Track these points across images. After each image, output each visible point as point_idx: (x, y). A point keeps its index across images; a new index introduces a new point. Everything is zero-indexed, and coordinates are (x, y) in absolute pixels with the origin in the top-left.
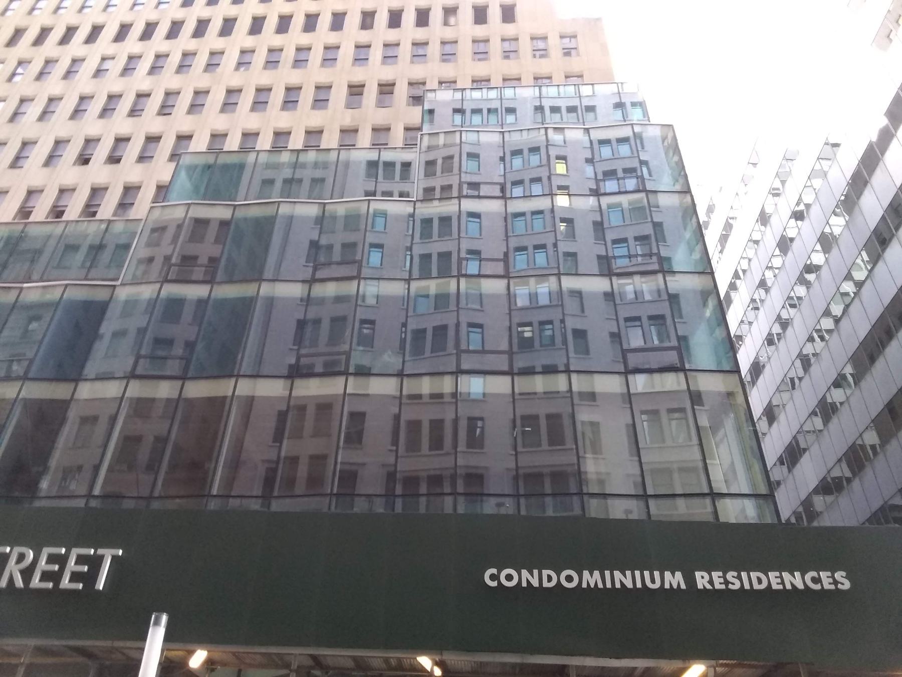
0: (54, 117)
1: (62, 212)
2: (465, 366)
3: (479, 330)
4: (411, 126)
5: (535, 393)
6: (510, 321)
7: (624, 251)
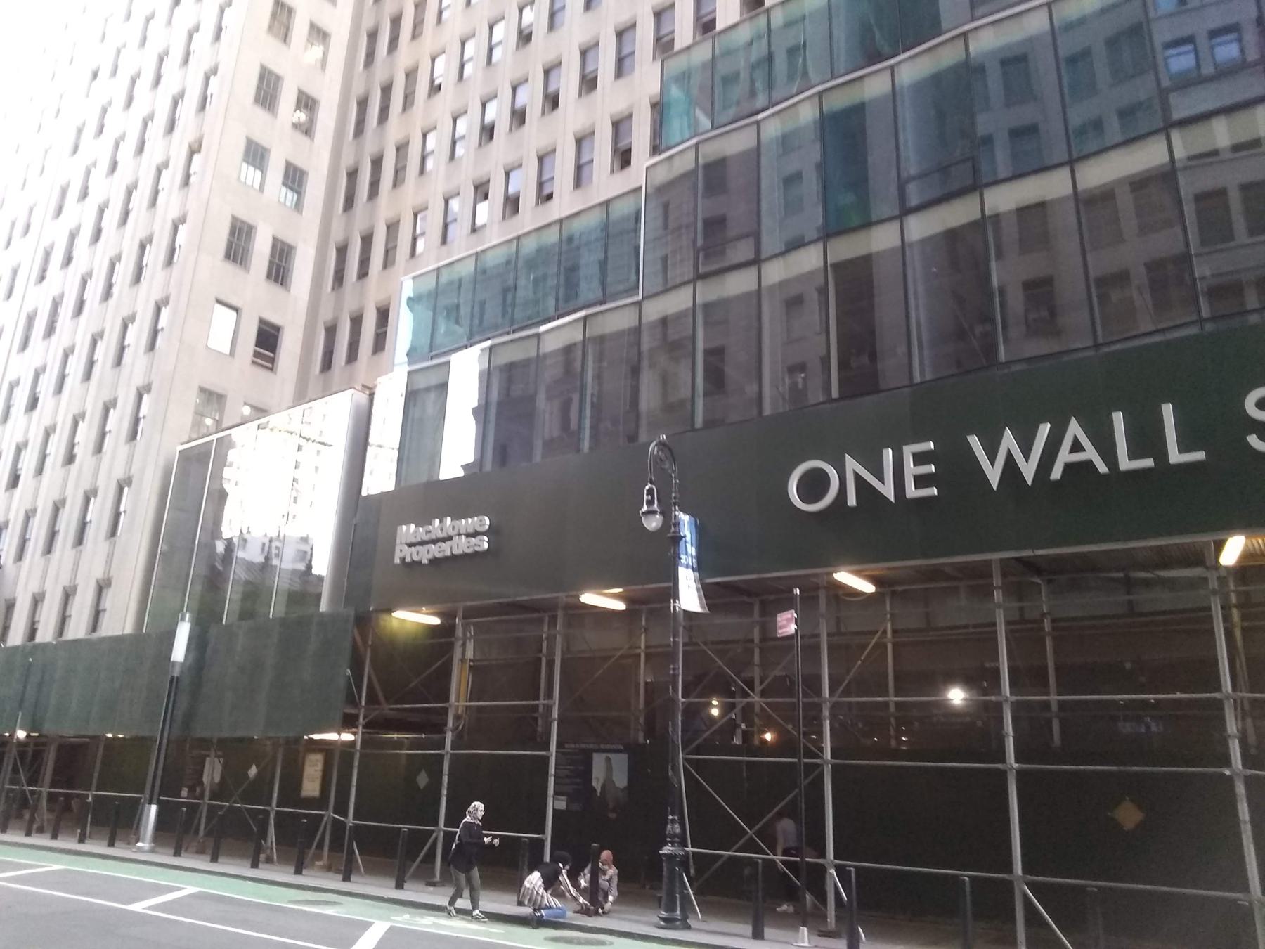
1: (713, 21)
3: (1190, 47)
5: (1215, 153)
6: (606, 252)
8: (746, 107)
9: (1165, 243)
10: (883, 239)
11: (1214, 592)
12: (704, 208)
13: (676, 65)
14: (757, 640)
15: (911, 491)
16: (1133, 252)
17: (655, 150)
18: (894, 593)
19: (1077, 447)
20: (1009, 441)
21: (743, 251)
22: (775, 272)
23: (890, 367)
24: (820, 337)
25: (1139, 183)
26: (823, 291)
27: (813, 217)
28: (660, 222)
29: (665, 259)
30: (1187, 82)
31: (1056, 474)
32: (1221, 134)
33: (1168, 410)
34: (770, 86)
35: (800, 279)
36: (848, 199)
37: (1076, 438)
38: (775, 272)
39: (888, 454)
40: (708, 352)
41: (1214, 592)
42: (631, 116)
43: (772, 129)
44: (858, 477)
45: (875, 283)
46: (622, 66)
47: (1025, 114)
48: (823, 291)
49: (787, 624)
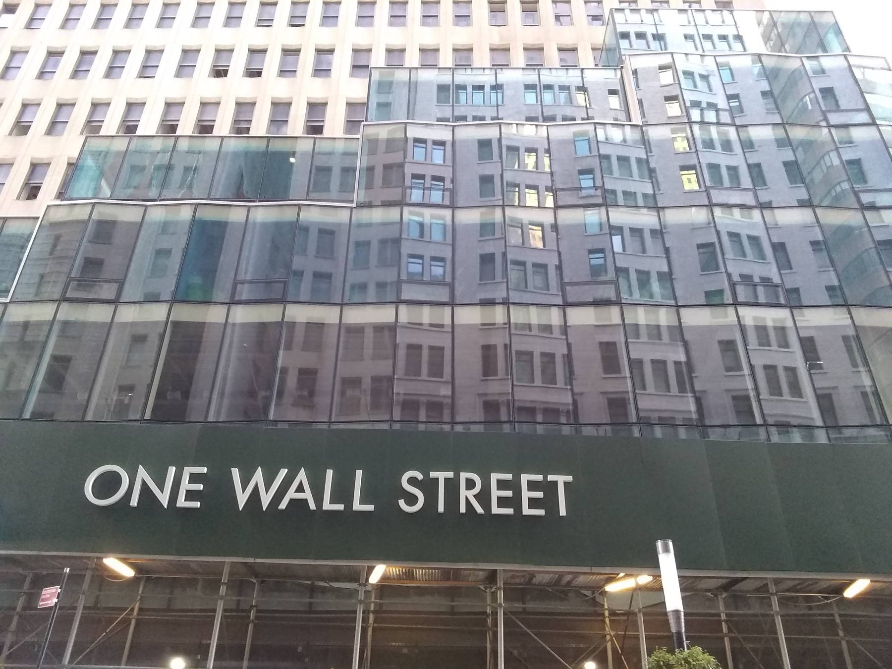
0: (44, 25)
2: (405, 296)
4: (564, 47)
5: (421, 324)
7: (590, 183)
8: (141, 194)
9: (383, 368)
10: (214, 315)
11: (361, 602)
12: (86, 249)
13: (96, 144)
14: (18, 609)
15: (181, 502)
16: (369, 368)
17: (60, 195)
18: (148, 579)
19: (300, 489)
20: (258, 476)
21: (107, 291)
22: (128, 314)
23: (196, 403)
24: (149, 367)
25: (379, 328)
26: (162, 337)
27: (167, 286)
28: (48, 249)
29: (42, 276)
30: (416, 280)
31: (283, 506)
32: (426, 315)
33: (359, 474)
34: (164, 184)
35: (145, 324)
36: (197, 280)
37: (301, 483)
38: (128, 314)
39: (172, 470)
40: (55, 358)
41: (361, 602)
42: (49, 164)
43: (157, 214)
44: (144, 483)
45: (204, 339)
46: (54, 127)
47: (324, 266)
48: (162, 337)
49: (50, 596)
